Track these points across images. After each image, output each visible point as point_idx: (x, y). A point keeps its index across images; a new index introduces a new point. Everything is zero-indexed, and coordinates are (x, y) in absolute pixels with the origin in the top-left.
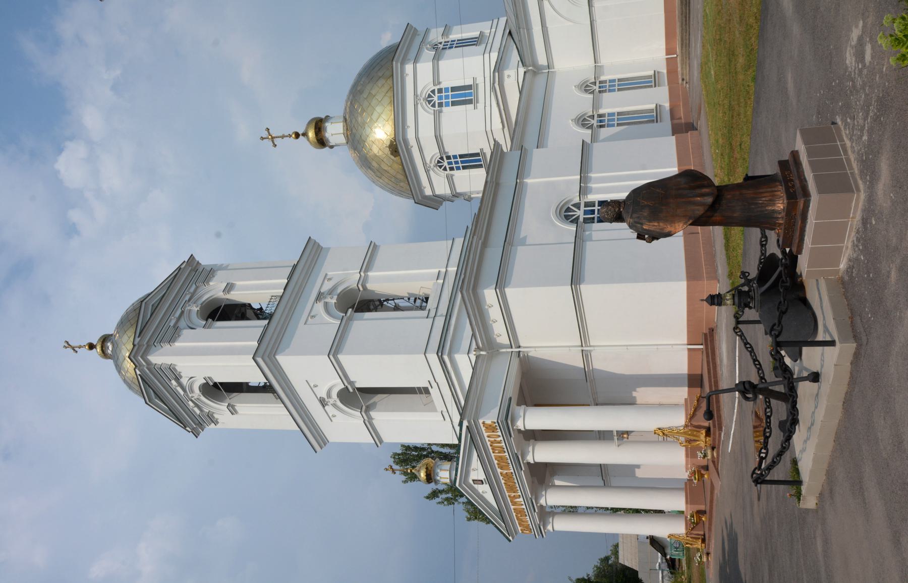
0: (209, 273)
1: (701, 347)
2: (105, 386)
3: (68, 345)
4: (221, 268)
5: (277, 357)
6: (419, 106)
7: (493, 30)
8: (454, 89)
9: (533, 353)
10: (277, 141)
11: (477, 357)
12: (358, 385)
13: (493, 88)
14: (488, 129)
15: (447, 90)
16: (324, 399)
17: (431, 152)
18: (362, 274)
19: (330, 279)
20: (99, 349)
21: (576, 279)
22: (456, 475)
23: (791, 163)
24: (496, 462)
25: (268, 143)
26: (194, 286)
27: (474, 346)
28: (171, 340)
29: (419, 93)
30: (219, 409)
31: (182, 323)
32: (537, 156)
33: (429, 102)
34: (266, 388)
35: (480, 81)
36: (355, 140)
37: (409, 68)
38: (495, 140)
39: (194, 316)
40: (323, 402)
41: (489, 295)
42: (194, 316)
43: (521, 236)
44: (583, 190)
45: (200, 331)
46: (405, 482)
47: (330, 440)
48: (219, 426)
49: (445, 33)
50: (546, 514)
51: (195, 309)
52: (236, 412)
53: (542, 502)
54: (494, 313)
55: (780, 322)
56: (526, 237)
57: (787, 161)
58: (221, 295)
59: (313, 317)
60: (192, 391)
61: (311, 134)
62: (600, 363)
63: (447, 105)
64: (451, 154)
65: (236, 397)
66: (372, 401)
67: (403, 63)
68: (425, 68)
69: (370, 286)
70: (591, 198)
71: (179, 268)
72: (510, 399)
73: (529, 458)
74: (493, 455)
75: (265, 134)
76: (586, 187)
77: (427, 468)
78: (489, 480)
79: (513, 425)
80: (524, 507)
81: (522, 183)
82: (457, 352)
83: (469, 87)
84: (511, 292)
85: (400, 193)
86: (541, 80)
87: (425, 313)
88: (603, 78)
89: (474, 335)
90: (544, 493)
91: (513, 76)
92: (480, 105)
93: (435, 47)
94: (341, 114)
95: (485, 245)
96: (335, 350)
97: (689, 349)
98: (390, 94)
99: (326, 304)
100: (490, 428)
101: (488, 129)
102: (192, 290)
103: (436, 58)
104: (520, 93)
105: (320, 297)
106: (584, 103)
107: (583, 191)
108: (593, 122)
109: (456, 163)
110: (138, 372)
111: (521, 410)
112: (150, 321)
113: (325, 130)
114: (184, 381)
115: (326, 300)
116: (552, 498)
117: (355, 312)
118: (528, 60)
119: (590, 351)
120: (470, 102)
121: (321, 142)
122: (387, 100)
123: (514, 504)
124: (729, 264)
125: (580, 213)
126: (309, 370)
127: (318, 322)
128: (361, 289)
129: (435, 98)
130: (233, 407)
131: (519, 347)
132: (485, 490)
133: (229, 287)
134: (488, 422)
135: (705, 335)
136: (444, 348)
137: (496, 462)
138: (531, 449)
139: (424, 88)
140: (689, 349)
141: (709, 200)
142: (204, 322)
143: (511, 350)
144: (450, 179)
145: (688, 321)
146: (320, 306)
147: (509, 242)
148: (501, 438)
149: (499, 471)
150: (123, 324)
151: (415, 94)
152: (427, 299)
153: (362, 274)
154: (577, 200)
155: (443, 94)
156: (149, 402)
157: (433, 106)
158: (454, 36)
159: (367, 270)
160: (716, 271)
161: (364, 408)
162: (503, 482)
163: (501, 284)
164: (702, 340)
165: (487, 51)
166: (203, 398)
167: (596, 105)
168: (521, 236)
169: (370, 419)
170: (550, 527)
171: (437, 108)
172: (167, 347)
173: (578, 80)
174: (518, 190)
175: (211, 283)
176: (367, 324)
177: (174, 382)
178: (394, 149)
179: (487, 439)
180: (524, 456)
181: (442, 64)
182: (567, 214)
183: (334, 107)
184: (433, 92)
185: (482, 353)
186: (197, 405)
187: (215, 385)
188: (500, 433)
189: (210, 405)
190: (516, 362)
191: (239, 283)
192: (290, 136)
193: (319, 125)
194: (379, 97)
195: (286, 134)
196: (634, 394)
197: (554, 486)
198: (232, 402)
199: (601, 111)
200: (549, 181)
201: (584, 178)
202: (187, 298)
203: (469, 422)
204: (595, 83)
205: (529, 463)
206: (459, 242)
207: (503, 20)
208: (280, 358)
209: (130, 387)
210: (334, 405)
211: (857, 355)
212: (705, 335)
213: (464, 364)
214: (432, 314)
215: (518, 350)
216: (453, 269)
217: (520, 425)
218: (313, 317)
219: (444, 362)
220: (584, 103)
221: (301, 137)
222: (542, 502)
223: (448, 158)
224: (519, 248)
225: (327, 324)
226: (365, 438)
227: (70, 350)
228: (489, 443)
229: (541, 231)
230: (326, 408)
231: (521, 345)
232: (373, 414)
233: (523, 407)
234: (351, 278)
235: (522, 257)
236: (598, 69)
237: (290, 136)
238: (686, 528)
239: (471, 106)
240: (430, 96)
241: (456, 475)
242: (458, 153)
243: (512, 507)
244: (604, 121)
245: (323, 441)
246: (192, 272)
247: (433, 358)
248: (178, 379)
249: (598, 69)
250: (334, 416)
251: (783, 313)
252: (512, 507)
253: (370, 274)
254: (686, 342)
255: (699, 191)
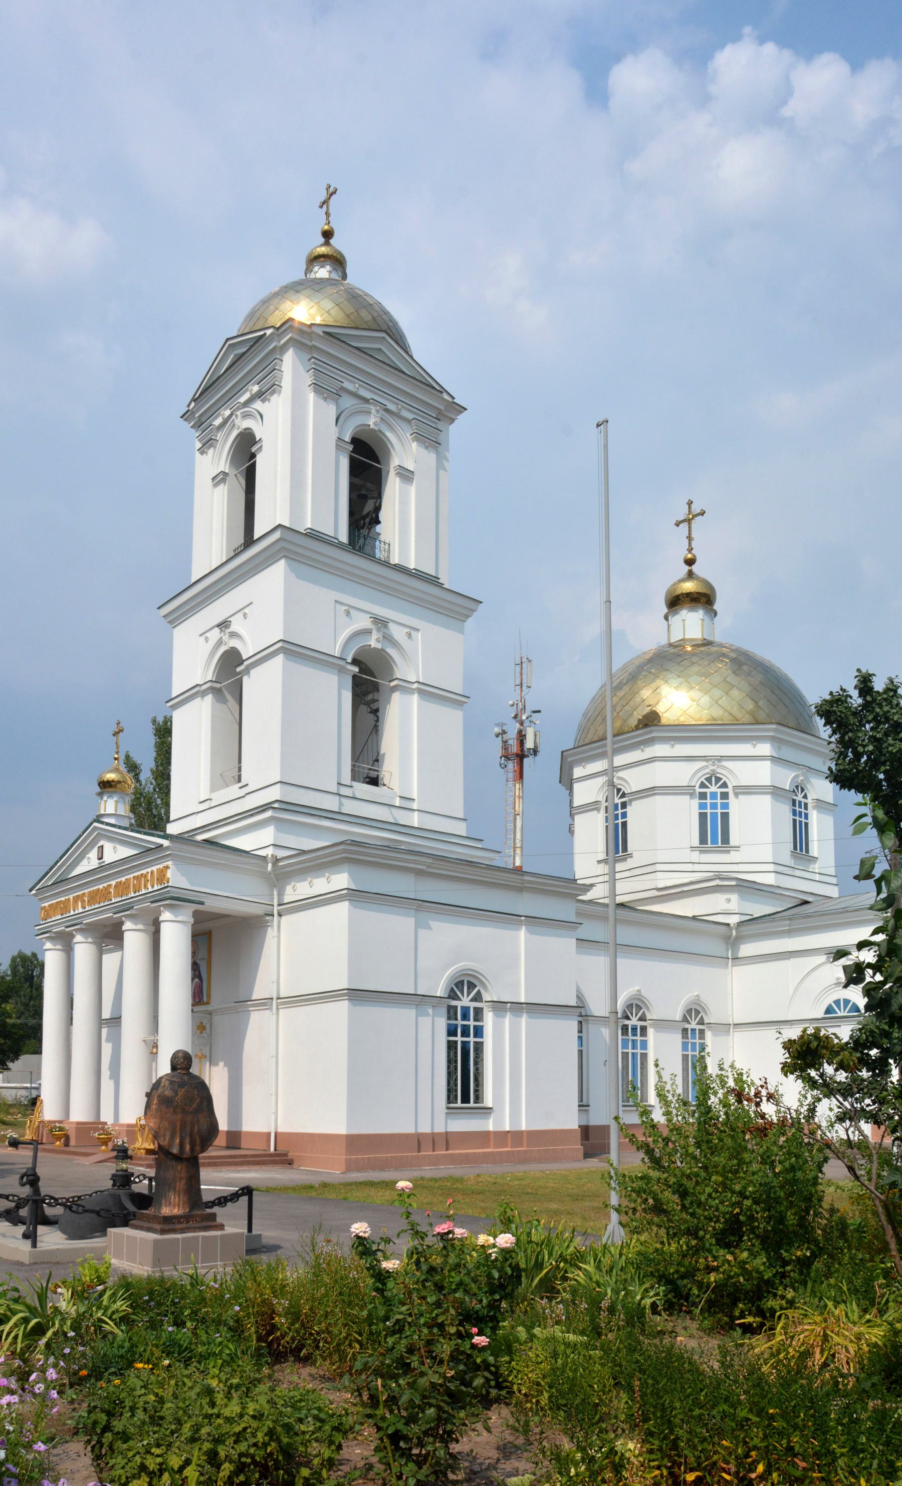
0: (432, 440)
1: (272, 1149)
2: (252, 275)
3: (332, 193)
4: (441, 461)
5: (283, 561)
6: (705, 763)
7: (817, 877)
8: (725, 817)
9: (271, 933)
10: (684, 527)
11: (264, 858)
12: (245, 679)
13: (719, 876)
14: (659, 867)
15: (726, 806)
16: (228, 627)
17: (633, 780)
18: (415, 686)
19: (409, 636)
20: (323, 250)
21: (356, 995)
22: (107, 824)
23: (215, 1223)
24: (123, 879)
25: (682, 513)
26: (410, 416)
27: (281, 853)
28: (318, 388)
29: (724, 763)
30: (219, 459)
31: (348, 402)
32: (565, 944)
33: (709, 780)
34: (249, 540)
35: (733, 856)
36: (669, 659)
37: (765, 749)
38: (592, 885)
39: (359, 420)
40: (223, 625)
41: (341, 880)
42: (359, 420)
43: (431, 923)
44: (499, 1006)
45: (333, 432)
46: (154, 721)
47: (176, 631)
48: (197, 453)
49: (821, 804)
50: (66, 942)
51: (372, 421)
52: (216, 485)
53: (78, 938)
54: (321, 885)
55: (86, 1211)
56: (429, 928)
57: (215, 1220)
58: (395, 461)
59: (348, 613)
60: (246, 416)
61: (689, 586)
62: (258, 1023)
63: (702, 806)
64: (629, 809)
65: (238, 484)
66: (228, 696)
67: (773, 740)
68: (762, 773)
69: (396, 697)
70: (489, 1017)
71: (442, 390)
72: (202, 903)
73: (128, 925)
74: (131, 876)
75: (696, 509)
76: (505, 1010)
77: (119, 782)
78: (101, 868)
79: (166, 906)
80: (72, 913)
81: (520, 923)
82: (278, 829)
83: (726, 839)
84: (343, 908)
85: (583, 729)
86: (716, 947)
87: (347, 777)
88: (708, 1034)
89: (304, 852)
90: (90, 940)
91: (726, 907)
92: (696, 856)
93: (799, 788)
94: (718, 638)
95: (419, 873)
96: (290, 650)
97: (269, 1134)
98: (727, 719)
99: (368, 632)
100: (162, 874)
101: (659, 867)
102: (405, 413)
103: (776, 791)
104: (694, 918)
105: (381, 623)
106: (667, 1005)
107: (499, 1006)
108: (632, 1021)
109: (714, 806)
110: (269, 332)
111: (186, 915)
112: (361, 344)
113: (692, 609)
114: (258, 405)
115: (374, 632)
116: (83, 950)
117: (354, 677)
118: (745, 929)
119: (271, 1009)
120: (703, 840)
121: (675, 602)
122: (717, 713)
123: (76, 899)
124: (341, 1184)
125: (465, 1001)
126: (264, 609)
127: (338, 618)
128: (393, 684)
129: (713, 788)
130: (223, 480)
131: (280, 915)
132: (90, 862)
133: (406, 475)
134: (169, 874)
135: (286, 1155)
136: (284, 811)
137: (123, 879)
138: (140, 927)
139: (731, 772)
140: (269, 1134)
141: (175, 1150)
142: (348, 438)
143: (275, 903)
144: (593, 806)
145: (303, 1135)
146: (364, 622)
147: (422, 906)
148: (150, 890)
149: (113, 883)
150: (357, 300)
151: (721, 758)
152: (374, 781)
153: (415, 686)
154: (486, 997)
155: (719, 801)
156: (230, 344)
157: (702, 785)
158: (814, 817)
159: (421, 692)
160: (358, 1170)
161: (218, 686)
162: (101, 887)
163: (354, 895)
164: (281, 1149)
165: (780, 868)
166: (235, 433)
167: (663, 1024)
168: (431, 923)
169: (203, 694)
170: (48, 945)
171: (698, 790)
172: (308, 379)
173: (708, 1000)
174: (511, 918)
175: (414, 445)
176: (334, 696)
177: (256, 388)
178: (651, 720)
179: (149, 870)
180: (131, 917)
181: (766, 800)
182: (465, 983)
183: (729, 624)
184: (725, 785)
185: (270, 865)
186: (225, 421)
187: (253, 456)
188: (156, 888)
189: (226, 442)
190: (258, 910)
191: (413, 490)
192: (690, 550)
193: (703, 599)
194: (724, 701)
195: (693, 544)
196: (221, 1064)
197: (100, 953)
198: (231, 479)
199: (651, 1032)
200: (519, 960)
201: (517, 1007)
202: (391, 406)
203: (168, 848)
204: (701, 1022)
205: (122, 923)
206: (461, 829)
207: (834, 892)
208: (280, 566)
209: (251, 316)
210: (220, 642)
211: (20, 1264)
212: (286, 1155)
213: (258, 840)
214: (344, 791)
215: (275, 913)
216: (415, 820)
217: (166, 915)
218: (348, 613)
219: (264, 811)
220: (667, 1005)
221: (687, 568)
222: (78, 938)
223: (624, 805)
224: (412, 921)
225: (336, 635)
226: (178, 687)
227: (323, 196)
228: (144, 872)
229: (442, 949)
230: (217, 630)
231: (283, 918)
232: (209, 698)
233: (192, 920)
234: (408, 669)
235: (397, 925)
236: (725, 1028)
237: (690, 550)
238: (50, 1122)
239: (696, 842)
240: (718, 779)
241: (107, 824)
242: (629, 819)
243: (71, 897)
244: (635, 1035)
245: (175, 619)
246: (435, 410)
247: (274, 794)
248: (260, 395)
249: (725, 1028)
250: (207, 639)
251: (98, 1213)
252: (71, 897)
253: (415, 697)
254: (279, 1130)
255: (187, 1140)
